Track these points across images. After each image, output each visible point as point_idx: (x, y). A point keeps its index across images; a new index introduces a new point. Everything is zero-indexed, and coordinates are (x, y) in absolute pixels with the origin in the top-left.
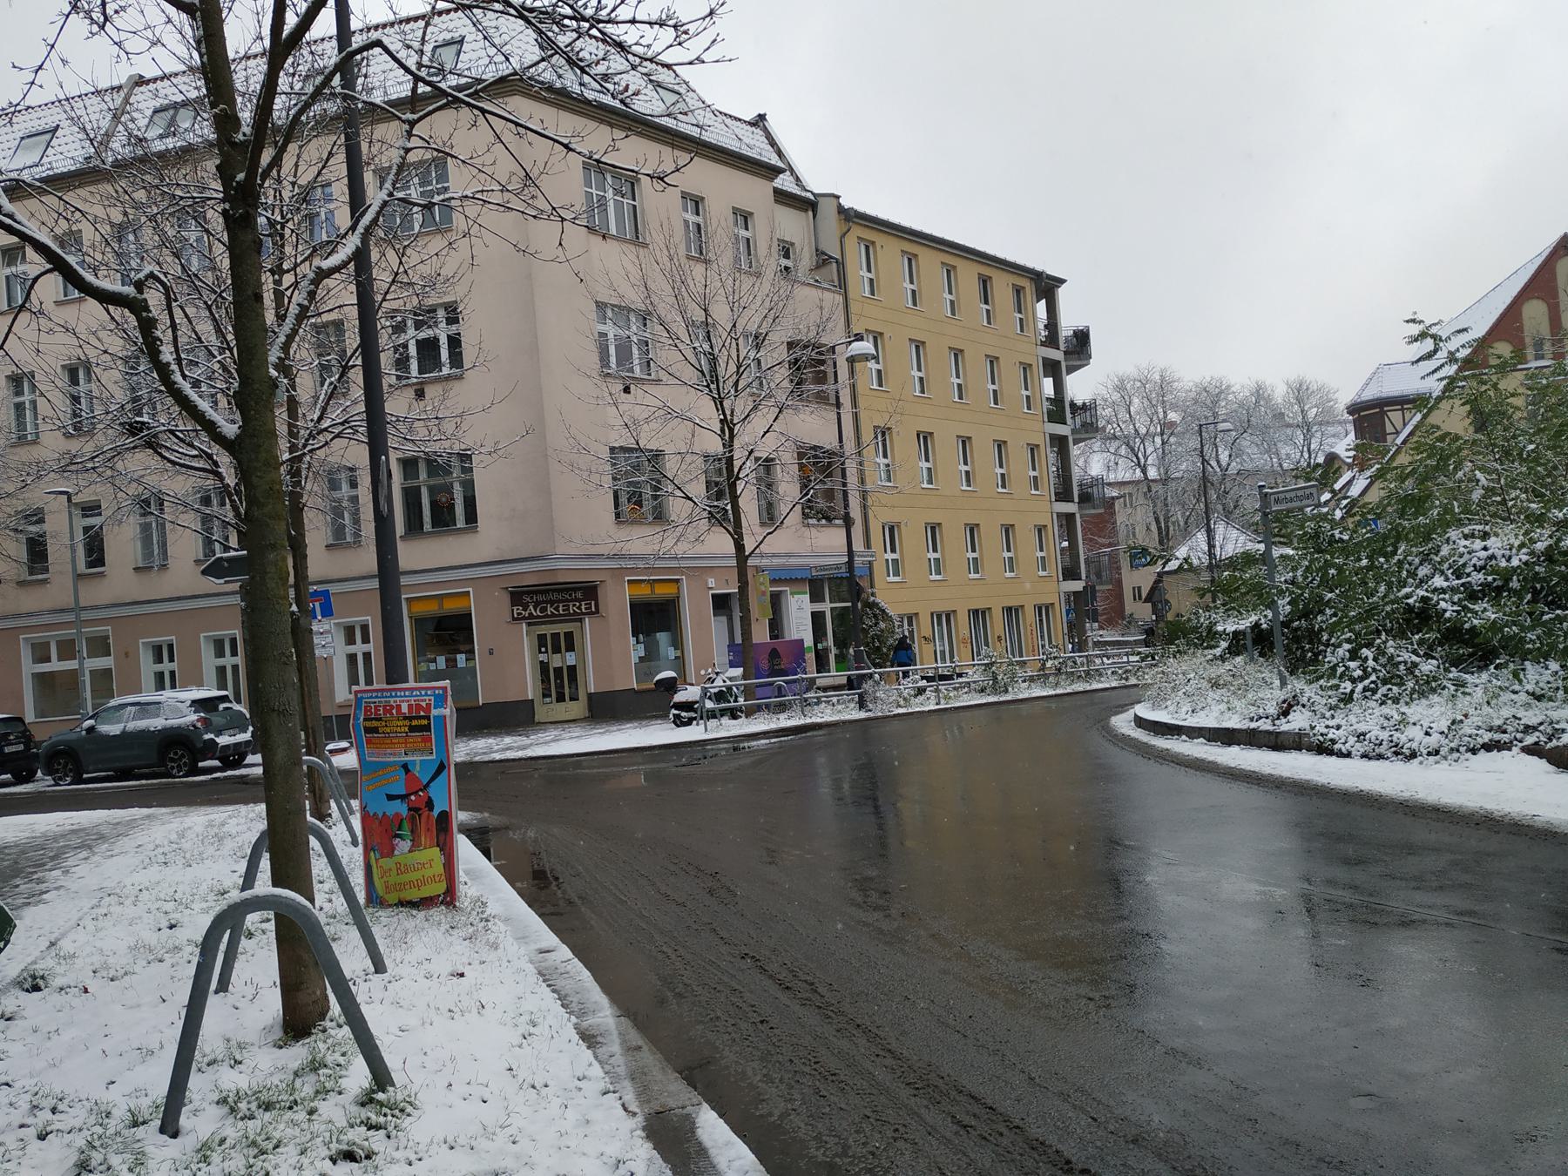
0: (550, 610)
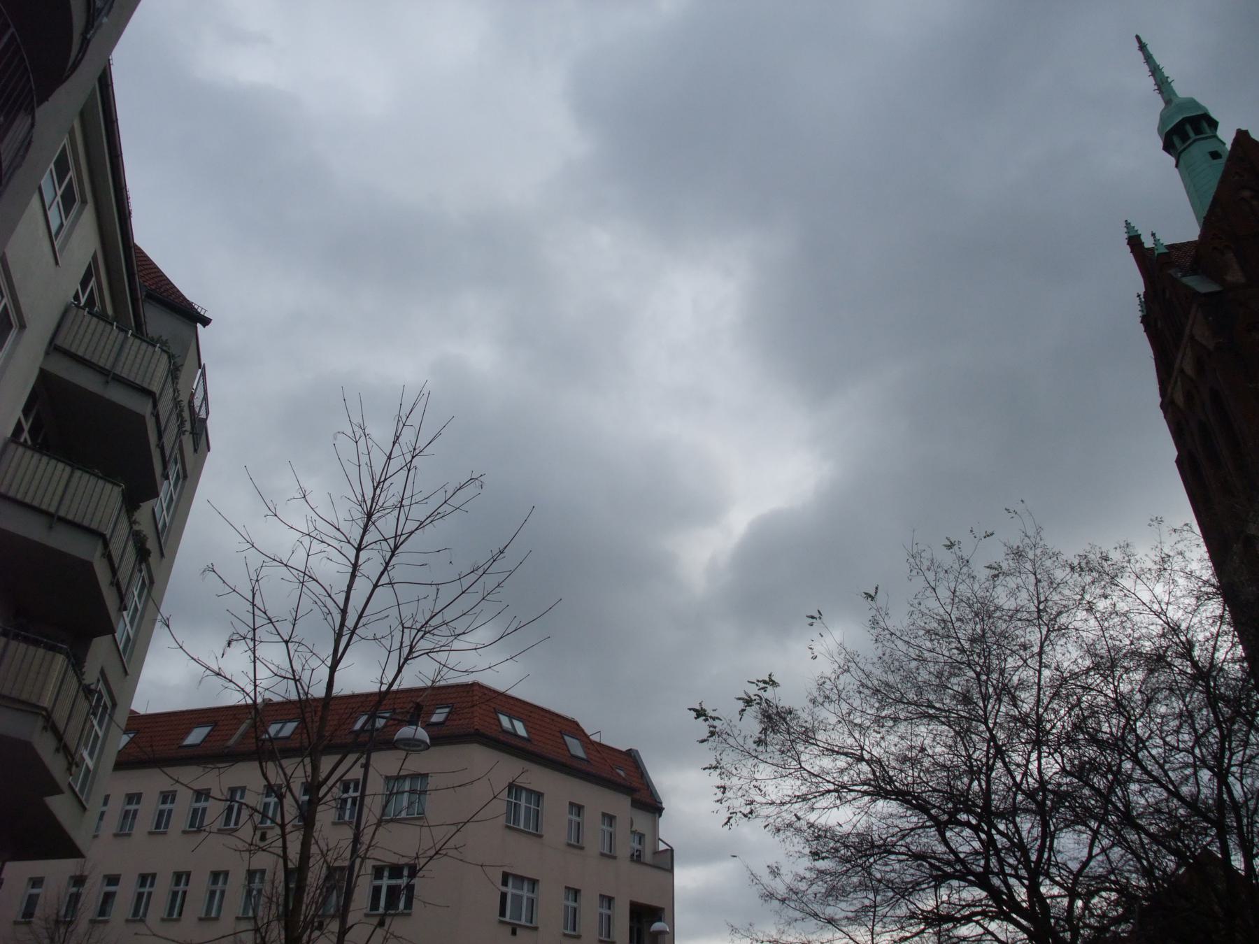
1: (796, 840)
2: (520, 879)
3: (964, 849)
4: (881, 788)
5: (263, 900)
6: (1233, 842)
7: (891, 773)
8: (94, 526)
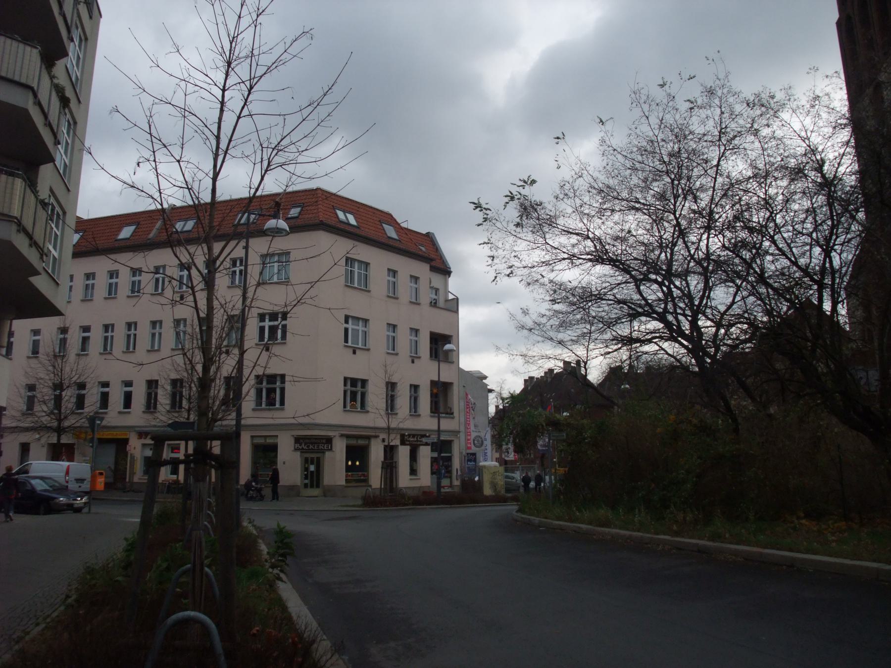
0: (311, 447)
1: (541, 290)
2: (357, 319)
3: (651, 297)
4: (600, 257)
5: (187, 337)
6: (826, 295)
7: (607, 247)
8: (23, 81)
